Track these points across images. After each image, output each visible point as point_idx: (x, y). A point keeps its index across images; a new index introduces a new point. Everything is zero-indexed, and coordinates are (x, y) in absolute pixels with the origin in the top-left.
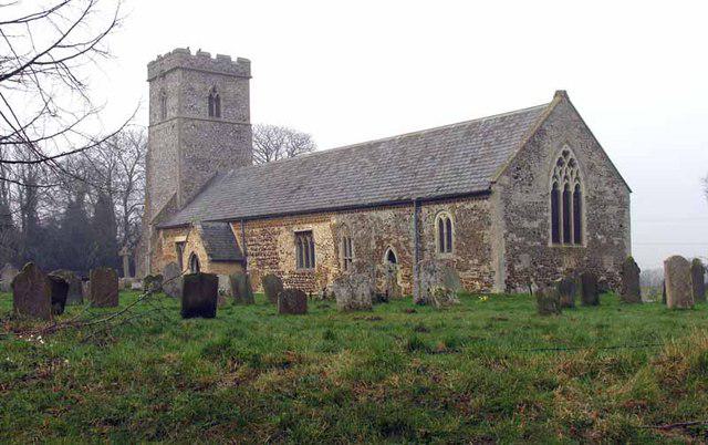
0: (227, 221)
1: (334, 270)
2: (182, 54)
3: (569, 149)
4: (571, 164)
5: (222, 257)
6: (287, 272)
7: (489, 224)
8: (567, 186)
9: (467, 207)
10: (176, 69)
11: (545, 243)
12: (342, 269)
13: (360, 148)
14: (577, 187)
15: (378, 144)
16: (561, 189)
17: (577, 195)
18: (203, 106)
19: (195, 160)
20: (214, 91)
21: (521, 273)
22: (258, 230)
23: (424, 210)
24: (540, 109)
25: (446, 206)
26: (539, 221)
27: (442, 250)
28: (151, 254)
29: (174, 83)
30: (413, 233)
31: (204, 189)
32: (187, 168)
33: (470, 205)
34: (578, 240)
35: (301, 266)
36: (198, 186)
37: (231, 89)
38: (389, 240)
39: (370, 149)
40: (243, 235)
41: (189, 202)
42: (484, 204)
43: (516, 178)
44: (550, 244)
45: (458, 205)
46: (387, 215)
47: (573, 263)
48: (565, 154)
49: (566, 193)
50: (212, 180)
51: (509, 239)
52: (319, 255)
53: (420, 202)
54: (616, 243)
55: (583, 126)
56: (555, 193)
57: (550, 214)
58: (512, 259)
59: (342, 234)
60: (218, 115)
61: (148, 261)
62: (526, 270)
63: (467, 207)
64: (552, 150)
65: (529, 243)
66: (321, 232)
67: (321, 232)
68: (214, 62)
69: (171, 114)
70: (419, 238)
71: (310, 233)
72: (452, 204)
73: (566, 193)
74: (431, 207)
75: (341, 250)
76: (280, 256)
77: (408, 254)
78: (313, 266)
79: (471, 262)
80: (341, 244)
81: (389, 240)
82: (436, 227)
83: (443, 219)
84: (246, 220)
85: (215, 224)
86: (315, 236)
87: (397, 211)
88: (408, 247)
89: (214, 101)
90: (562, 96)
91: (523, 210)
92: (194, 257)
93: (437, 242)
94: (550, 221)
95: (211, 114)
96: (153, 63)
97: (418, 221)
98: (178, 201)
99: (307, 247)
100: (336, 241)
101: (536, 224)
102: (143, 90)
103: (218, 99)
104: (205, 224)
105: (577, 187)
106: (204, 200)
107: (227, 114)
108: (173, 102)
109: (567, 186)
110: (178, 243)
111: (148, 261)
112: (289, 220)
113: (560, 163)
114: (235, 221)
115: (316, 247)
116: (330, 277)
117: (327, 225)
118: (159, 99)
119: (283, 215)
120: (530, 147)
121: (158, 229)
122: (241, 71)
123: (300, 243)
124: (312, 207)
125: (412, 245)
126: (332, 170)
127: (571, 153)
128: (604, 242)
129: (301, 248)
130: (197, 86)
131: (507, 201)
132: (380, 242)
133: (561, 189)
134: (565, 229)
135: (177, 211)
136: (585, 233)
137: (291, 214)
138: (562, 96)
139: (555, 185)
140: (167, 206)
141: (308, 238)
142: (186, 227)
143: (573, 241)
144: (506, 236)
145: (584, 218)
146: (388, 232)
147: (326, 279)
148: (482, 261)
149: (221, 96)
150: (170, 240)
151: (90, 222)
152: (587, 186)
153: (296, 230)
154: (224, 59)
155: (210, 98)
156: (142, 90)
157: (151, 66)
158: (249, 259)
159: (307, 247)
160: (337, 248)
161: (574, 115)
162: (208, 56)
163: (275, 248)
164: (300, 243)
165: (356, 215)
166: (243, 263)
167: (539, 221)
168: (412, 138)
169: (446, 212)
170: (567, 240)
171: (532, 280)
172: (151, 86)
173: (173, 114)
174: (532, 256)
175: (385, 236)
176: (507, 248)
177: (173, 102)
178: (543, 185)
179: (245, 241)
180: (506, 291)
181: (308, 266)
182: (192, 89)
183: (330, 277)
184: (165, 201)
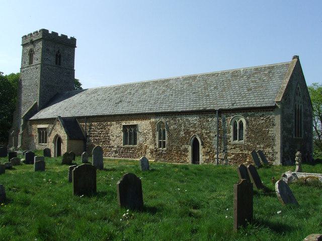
2: (45, 32)
7: (274, 125)
12: (157, 147)
17: (301, 110)
20: (58, 52)
22: (96, 123)
24: (71, 71)
27: (235, 139)
34: (301, 136)
38: (194, 132)
44: (294, 137)
46: (194, 119)
52: (140, 139)
57: (294, 120)
60: (60, 65)
63: (22, 124)
66: (144, 126)
67: (144, 126)
69: (35, 62)
71: (135, 126)
75: (157, 136)
76: (111, 137)
78: (135, 143)
79: (258, 146)
88: (209, 136)
93: (232, 134)
94: (294, 125)
95: (56, 64)
96: (26, 36)
103: (60, 56)
116: (148, 151)
118: (29, 56)
122: (71, 44)
130: (51, 49)
132: (187, 132)
134: (239, 134)
149: (62, 54)
153: (124, 124)
154: (64, 37)
155: (57, 55)
157: (25, 37)
161: (211, 79)
162: (57, 34)
175: (192, 129)
183: (148, 151)
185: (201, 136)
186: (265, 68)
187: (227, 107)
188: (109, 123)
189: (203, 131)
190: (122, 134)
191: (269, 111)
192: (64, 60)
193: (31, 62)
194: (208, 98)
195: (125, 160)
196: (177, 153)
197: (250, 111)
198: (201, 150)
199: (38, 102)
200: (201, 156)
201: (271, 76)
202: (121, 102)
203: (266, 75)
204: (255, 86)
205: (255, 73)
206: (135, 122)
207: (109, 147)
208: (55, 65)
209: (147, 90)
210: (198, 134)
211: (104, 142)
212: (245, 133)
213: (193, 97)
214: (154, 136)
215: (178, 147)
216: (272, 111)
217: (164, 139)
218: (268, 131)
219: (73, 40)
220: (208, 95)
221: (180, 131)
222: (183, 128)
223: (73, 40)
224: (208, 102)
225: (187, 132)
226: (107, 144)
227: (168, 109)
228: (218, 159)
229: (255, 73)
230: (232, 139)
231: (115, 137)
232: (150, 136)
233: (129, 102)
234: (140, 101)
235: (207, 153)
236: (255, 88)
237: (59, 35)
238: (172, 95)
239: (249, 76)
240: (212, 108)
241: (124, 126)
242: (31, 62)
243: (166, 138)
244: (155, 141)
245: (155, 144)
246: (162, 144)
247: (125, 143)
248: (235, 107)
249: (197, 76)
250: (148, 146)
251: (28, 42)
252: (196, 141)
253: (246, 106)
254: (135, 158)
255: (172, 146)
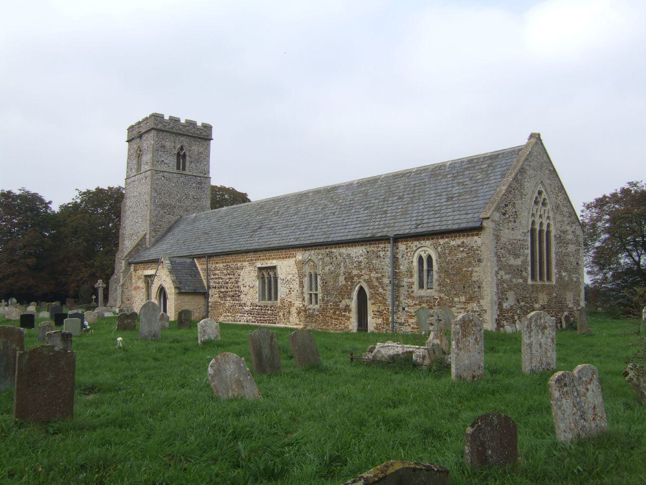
0: (193, 257)
1: (298, 304)
2: (157, 117)
3: (542, 189)
4: (544, 204)
5: (187, 289)
6: (249, 304)
7: (480, 261)
8: (541, 224)
9: (453, 243)
10: (153, 129)
11: (525, 280)
12: (306, 303)
13: (317, 192)
14: (548, 225)
15: (334, 188)
16: (537, 227)
17: (548, 232)
18: (172, 161)
19: (163, 206)
20: (182, 149)
21: (507, 311)
23: (402, 247)
24: (515, 152)
25: (428, 243)
26: (522, 258)
27: (421, 286)
28: (123, 285)
29: (149, 141)
30: (388, 270)
31: (170, 229)
32: (157, 212)
33: (455, 242)
34: (549, 279)
35: (263, 298)
36: (166, 226)
37: (196, 148)
38: (359, 276)
39: (330, 192)
40: (207, 270)
41: (157, 241)
42: (475, 241)
43: (504, 214)
44: (530, 282)
45: (442, 241)
46: (358, 252)
47: (546, 299)
48: (540, 193)
49: (541, 231)
50: (177, 222)
51: (499, 277)
52: (282, 290)
53: (397, 239)
54: (575, 279)
55: (552, 169)
56: (533, 231)
57: (529, 252)
58: (501, 296)
59: (307, 269)
60: (184, 169)
61: (119, 291)
62: (512, 307)
63: (453, 243)
64: (530, 188)
65: (514, 280)
66: (286, 267)
67: (286, 267)
68: (184, 126)
69: (145, 167)
70: (395, 275)
71: (274, 268)
72: (434, 241)
73: (541, 231)
74: (410, 243)
76: (242, 289)
77: (381, 290)
78: (276, 299)
79: (456, 299)
80: (306, 280)
81: (359, 276)
82: (415, 264)
83: (424, 256)
84: (210, 256)
85: (184, 259)
86: (279, 271)
87: (372, 248)
88: (381, 283)
89: (181, 157)
90: (536, 138)
91: (510, 247)
92: (162, 291)
93: (415, 279)
94: (529, 259)
95: (178, 168)
96: (132, 127)
97: (395, 260)
98: (147, 240)
99: (270, 281)
100: (301, 276)
101: (518, 262)
102: (123, 148)
103: (184, 155)
104: (172, 259)
105: (548, 225)
106: (170, 240)
107: (190, 168)
108: (147, 157)
109: (541, 224)
110: (146, 276)
111: (119, 291)
112: (251, 256)
113: (536, 203)
114: (199, 257)
115: (279, 281)
117: (292, 261)
118: (136, 156)
119: (247, 252)
120: (515, 185)
121: (130, 264)
123: (263, 278)
124: (275, 244)
125: (386, 281)
126: (291, 211)
127: (544, 193)
128: (566, 279)
129: (263, 283)
130: (168, 144)
131: (497, 237)
132: (349, 278)
133: (537, 227)
134: (423, 281)
135: (146, 248)
136: (554, 270)
137: (255, 251)
138: (536, 138)
139: (533, 223)
140: (138, 245)
141: (272, 274)
142: (156, 262)
143: (538, 280)
144: (497, 273)
145: (553, 256)
146: (359, 267)
147: (289, 312)
148: (471, 299)
149: (187, 153)
150: (140, 272)
151: (401, 356)
152: (555, 225)
153: (260, 266)
154: (191, 124)
155: (178, 154)
156: (121, 148)
157: (131, 129)
158: (211, 292)
159: (270, 281)
160: (301, 283)
163: (237, 282)
164: (263, 278)
165: (323, 251)
166: (206, 295)
167: (522, 258)
168: (372, 182)
169: (427, 249)
170: (541, 278)
171: (516, 317)
172: (130, 145)
173: (147, 167)
174: (516, 294)
175: (355, 272)
176: (497, 285)
177: (147, 157)
178: (524, 222)
179: (208, 275)
180: (496, 329)
181: (270, 299)
182: (164, 147)
183: (294, 310)
184: (135, 240)
185: (369, 282)
186: (484, 158)
187: (407, 232)
188: (239, 264)
189: (372, 275)
190: (257, 283)
191: (473, 235)
192: (191, 162)
193: (139, 169)
194: (384, 216)
195: (15, 361)
196: (334, 313)
197: (442, 238)
198: (371, 308)
199: (148, 232)
200: (369, 318)
201: (489, 172)
202: (260, 228)
203: (482, 170)
204: (461, 191)
205: (467, 169)
206: (274, 263)
207: (240, 305)
208: (175, 170)
209: (302, 207)
210: (365, 280)
211: (233, 296)
212: (435, 276)
213: (363, 215)
214: (301, 284)
215: (336, 304)
216: (477, 235)
217: (317, 290)
218: (472, 272)
219: (207, 128)
220: (385, 212)
221: (338, 276)
222: (342, 270)
223: (207, 128)
224: (382, 223)
225: (349, 278)
226: (237, 300)
227: (347, 236)
228: (393, 322)
229: (467, 169)
230: (415, 287)
231: (247, 287)
232: (296, 286)
233: (271, 228)
234: (287, 226)
235: (380, 313)
236: (460, 195)
237: (183, 121)
238: (334, 213)
239: (456, 174)
240: (384, 234)
241: (260, 269)
242: (139, 169)
243: (319, 288)
244: (302, 293)
245: (303, 299)
246: (313, 297)
247: (263, 297)
248: (419, 230)
249: (379, 179)
250: (293, 302)
251: (136, 134)
252: (361, 291)
253: (436, 229)
254: (275, 323)
255: (328, 301)
